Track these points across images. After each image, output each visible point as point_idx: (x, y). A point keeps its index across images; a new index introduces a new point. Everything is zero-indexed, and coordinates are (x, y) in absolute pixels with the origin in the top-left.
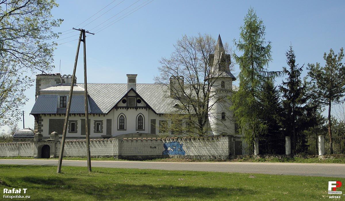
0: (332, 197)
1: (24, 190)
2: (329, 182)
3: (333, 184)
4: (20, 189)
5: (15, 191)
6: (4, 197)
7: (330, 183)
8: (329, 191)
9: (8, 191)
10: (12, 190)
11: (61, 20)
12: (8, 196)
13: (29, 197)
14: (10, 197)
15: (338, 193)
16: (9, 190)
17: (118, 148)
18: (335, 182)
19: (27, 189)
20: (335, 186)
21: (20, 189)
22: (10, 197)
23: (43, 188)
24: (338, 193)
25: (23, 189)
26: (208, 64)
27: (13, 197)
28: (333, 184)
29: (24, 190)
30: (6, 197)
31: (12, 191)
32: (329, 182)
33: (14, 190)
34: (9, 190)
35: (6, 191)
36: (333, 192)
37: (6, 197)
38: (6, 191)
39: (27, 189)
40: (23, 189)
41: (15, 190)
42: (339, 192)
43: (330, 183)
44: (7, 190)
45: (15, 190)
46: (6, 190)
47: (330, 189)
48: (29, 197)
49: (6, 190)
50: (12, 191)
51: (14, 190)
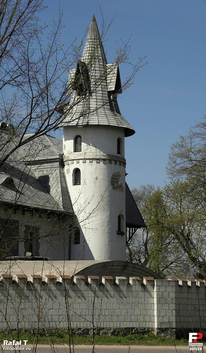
0: (193, 349)
1: (24, 342)
2: (190, 333)
3: (193, 336)
4: (20, 341)
5: (15, 343)
6: (5, 349)
7: (191, 334)
8: (190, 343)
9: (8, 343)
10: (12, 341)
11: (133, 82)
12: (8, 348)
13: (30, 349)
14: (10, 349)
15: (199, 345)
16: (9, 342)
17: (173, 306)
18: (196, 334)
19: (27, 341)
20: (196, 338)
21: (20, 341)
22: (10, 349)
23: (60, 341)
24: (199, 345)
25: (24, 341)
26: (83, 102)
27: (13, 349)
28: (193, 336)
29: (24, 342)
30: (6, 349)
31: (12, 343)
32: (190, 333)
33: (15, 342)
34: (9, 342)
35: (6, 343)
36: (193, 344)
37: (6, 349)
38: (6, 343)
39: (27, 341)
40: (24, 341)
41: (15, 341)
42: (200, 344)
43: (191, 334)
44: (7, 341)
45: (15, 341)
46: (6, 342)
47: (190, 341)
48: (30, 349)
49: (6, 342)
50: (12, 343)
51: (15, 342)
